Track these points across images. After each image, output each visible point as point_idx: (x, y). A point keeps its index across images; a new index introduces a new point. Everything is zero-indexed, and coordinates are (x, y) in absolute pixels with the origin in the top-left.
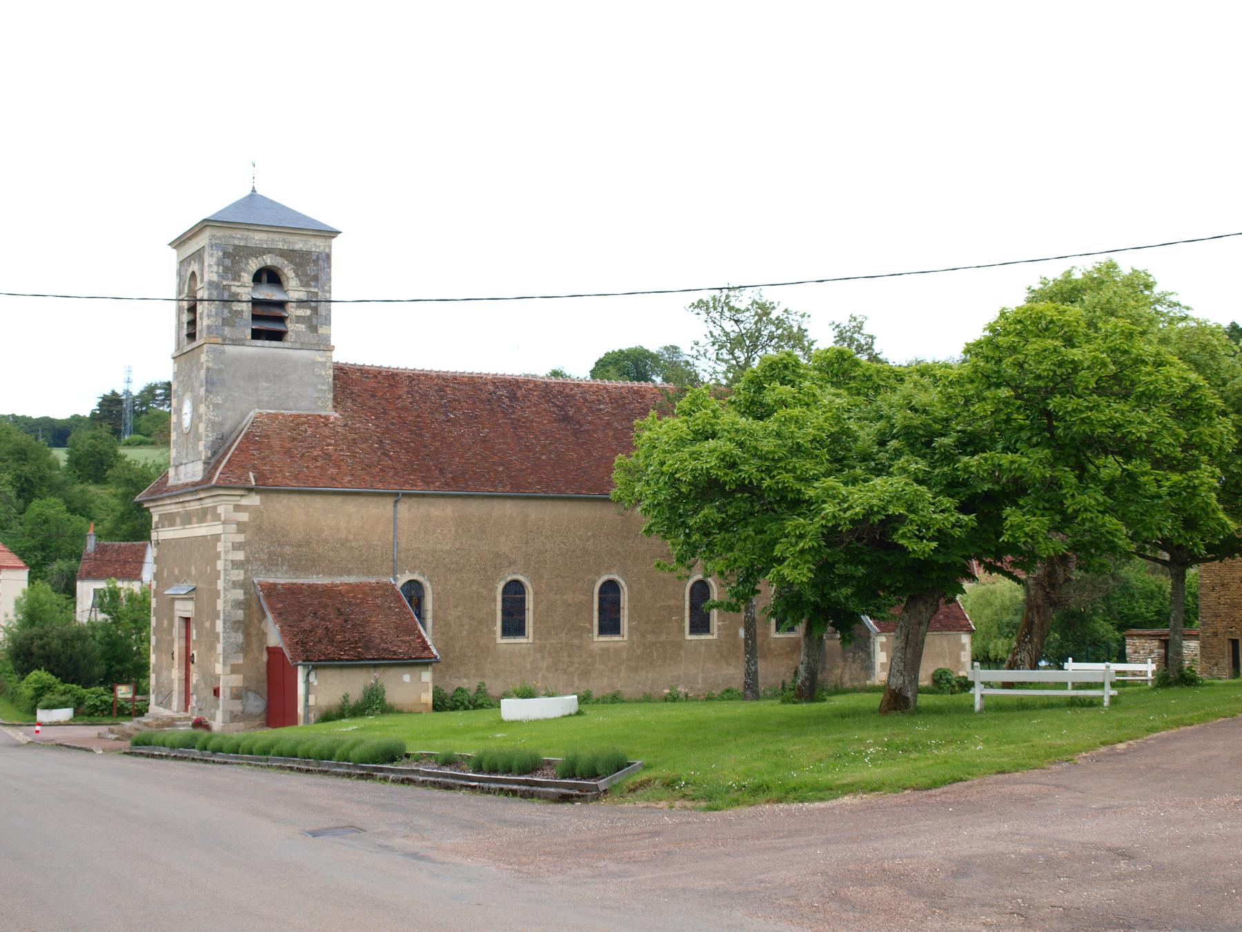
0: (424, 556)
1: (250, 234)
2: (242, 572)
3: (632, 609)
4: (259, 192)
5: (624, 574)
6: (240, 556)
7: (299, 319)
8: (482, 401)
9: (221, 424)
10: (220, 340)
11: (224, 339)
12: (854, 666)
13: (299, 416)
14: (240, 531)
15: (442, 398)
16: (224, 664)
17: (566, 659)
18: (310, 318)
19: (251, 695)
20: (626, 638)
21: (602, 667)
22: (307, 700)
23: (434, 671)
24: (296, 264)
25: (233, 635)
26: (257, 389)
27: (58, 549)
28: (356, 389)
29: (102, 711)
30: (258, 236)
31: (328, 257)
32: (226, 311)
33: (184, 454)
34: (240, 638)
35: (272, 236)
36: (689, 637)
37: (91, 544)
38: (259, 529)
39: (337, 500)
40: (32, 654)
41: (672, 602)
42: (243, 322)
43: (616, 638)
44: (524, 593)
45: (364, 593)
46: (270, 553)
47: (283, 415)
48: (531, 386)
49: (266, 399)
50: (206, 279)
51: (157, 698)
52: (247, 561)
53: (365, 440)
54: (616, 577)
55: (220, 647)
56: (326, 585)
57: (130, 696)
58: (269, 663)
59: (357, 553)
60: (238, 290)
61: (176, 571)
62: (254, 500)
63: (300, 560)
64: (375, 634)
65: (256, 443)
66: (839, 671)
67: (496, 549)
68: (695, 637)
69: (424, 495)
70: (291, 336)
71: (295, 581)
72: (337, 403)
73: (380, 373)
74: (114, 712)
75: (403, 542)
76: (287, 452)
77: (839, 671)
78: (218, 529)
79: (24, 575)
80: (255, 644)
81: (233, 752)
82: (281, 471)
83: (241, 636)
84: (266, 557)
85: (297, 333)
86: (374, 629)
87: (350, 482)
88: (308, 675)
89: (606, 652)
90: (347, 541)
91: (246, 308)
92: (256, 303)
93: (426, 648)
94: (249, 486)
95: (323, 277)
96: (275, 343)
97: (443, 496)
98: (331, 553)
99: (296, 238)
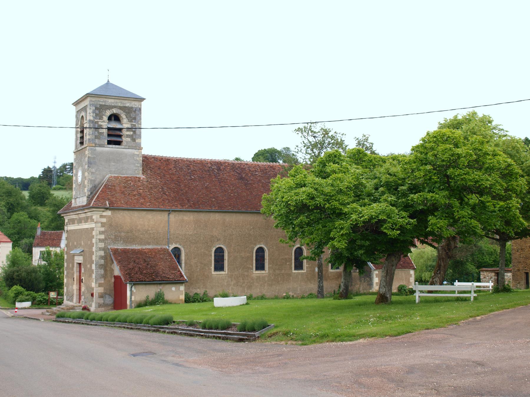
0: (181, 237)
1: (107, 100)
2: (103, 244)
3: (270, 259)
4: (110, 82)
5: (266, 245)
6: (102, 237)
7: (128, 136)
8: (206, 171)
9: (94, 181)
10: (94, 145)
11: (96, 145)
12: (364, 284)
13: (128, 177)
14: (102, 226)
15: (189, 169)
16: (96, 283)
17: (242, 281)
18: (132, 135)
19: (107, 296)
20: (267, 272)
21: (257, 284)
22: (131, 298)
23: (185, 286)
24: (126, 113)
25: (100, 270)
26: (110, 166)
27: (25, 234)
28: (152, 166)
29: (44, 303)
30: (110, 101)
31: (140, 109)
32: (96, 132)
33: (78, 193)
34: (102, 272)
35: (116, 100)
36: (294, 271)
37: (39, 232)
38: (111, 225)
39: (144, 213)
40: (14, 279)
41: (287, 257)
42: (103, 137)
43: (263, 272)
44: (224, 252)
45: (155, 253)
46: (115, 236)
47: (121, 177)
48: (227, 164)
49: (113, 170)
50: (88, 119)
51: (67, 297)
52: (106, 239)
53: (156, 188)
54: (263, 246)
55: (94, 276)
56: (139, 249)
57: (55, 296)
58: (115, 283)
59: (152, 236)
60: (102, 124)
61: (75, 243)
62: (109, 213)
63: (128, 239)
64: (160, 270)
65: (109, 189)
66: (358, 286)
67: (212, 234)
68: (296, 271)
69: (181, 211)
70: (124, 143)
71: (126, 247)
72: (144, 171)
73: (162, 159)
74: (49, 303)
75: (172, 231)
76: (123, 193)
77: (358, 286)
78: (93, 225)
79: (10, 245)
80: (109, 274)
81: (100, 320)
82: (120, 201)
83: (103, 271)
84: (114, 237)
85: (127, 142)
86: (160, 268)
87: (149, 205)
88: (131, 287)
89: (258, 278)
90: (148, 230)
91: (105, 131)
92: (109, 129)
93: (182, 276)
94: (106, 207)
95: (138, 118)
96: (117, 146)
97: (189, 211)
98: (141, 236)
99: (126, 101)
